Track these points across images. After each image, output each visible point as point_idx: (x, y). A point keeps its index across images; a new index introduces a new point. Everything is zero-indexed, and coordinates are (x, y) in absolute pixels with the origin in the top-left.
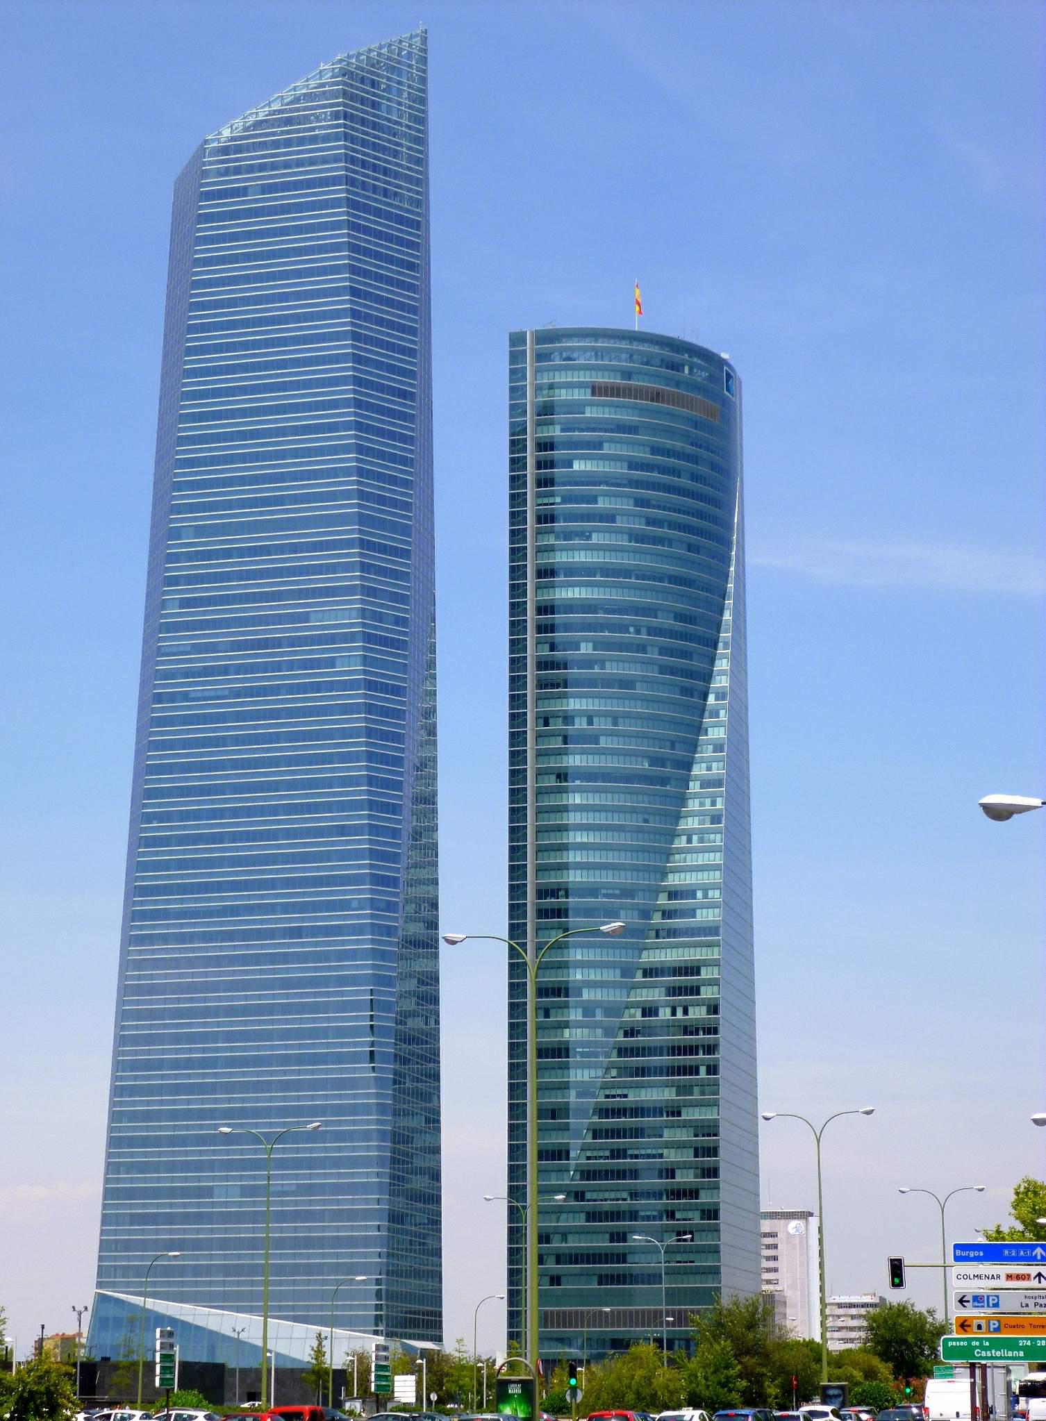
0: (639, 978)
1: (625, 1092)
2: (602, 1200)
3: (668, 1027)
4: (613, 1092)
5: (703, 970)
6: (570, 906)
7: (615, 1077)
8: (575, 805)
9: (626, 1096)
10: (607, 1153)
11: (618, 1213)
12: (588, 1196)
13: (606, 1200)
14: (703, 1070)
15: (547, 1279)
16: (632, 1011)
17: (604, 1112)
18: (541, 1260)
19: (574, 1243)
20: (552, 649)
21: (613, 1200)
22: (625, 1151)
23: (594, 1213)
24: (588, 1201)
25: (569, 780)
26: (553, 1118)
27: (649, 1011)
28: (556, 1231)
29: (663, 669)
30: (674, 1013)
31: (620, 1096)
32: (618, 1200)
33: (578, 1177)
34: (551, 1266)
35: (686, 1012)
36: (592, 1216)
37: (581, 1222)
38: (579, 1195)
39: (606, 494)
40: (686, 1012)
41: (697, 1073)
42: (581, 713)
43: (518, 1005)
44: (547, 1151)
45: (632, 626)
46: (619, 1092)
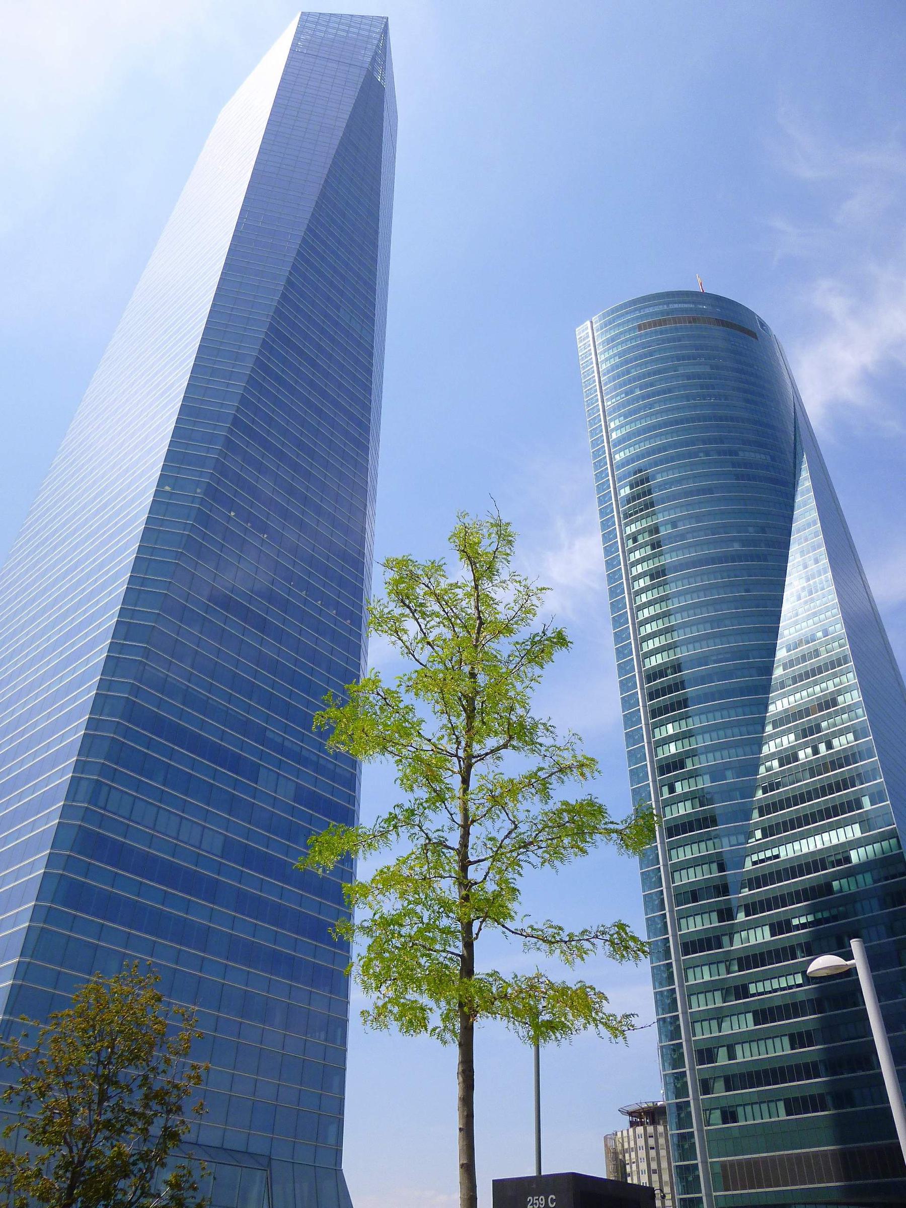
0: (741, 917)
1: (775, 852)
2: (770, 992)
3: (813, 769)
4: (762, 856)
5: (840, 699)
6: (718, 812)
7: (760, 839)
8: (765, 942)
9: (777, 857)
10: (623, 395)
11: (794, 1005)
12: (752, 989)
13: (775, 991)
14: (866, 801)
15: (716, 1115)
16: (768, 764)
17: (755, 882)
18: (706, 1087)
19: (745, 1055)
20: (722, 868)
21: (784, 989)
22: (788, 922)
23: (763, 1011)
24: (753, 995)
25: (667, 573)
26: (695, 900)
27: (788, 757)
28: (719, 1042)
29: (738, 477)
30: (816, 751)
31: (769, 859)
32: (790, 987)
33: (736, 968)
34: (719, 1092)
35: (829, 746)
36: (761, 1016)
37: (747, 1024)
38: (742, 991)
39: (661, 472)
40: (829, 746)
41: (860, 806)
42: (665, 523)
43: (687, 1167)
44: (693, 943)
45: (701, 452)
46: (769, 854)
